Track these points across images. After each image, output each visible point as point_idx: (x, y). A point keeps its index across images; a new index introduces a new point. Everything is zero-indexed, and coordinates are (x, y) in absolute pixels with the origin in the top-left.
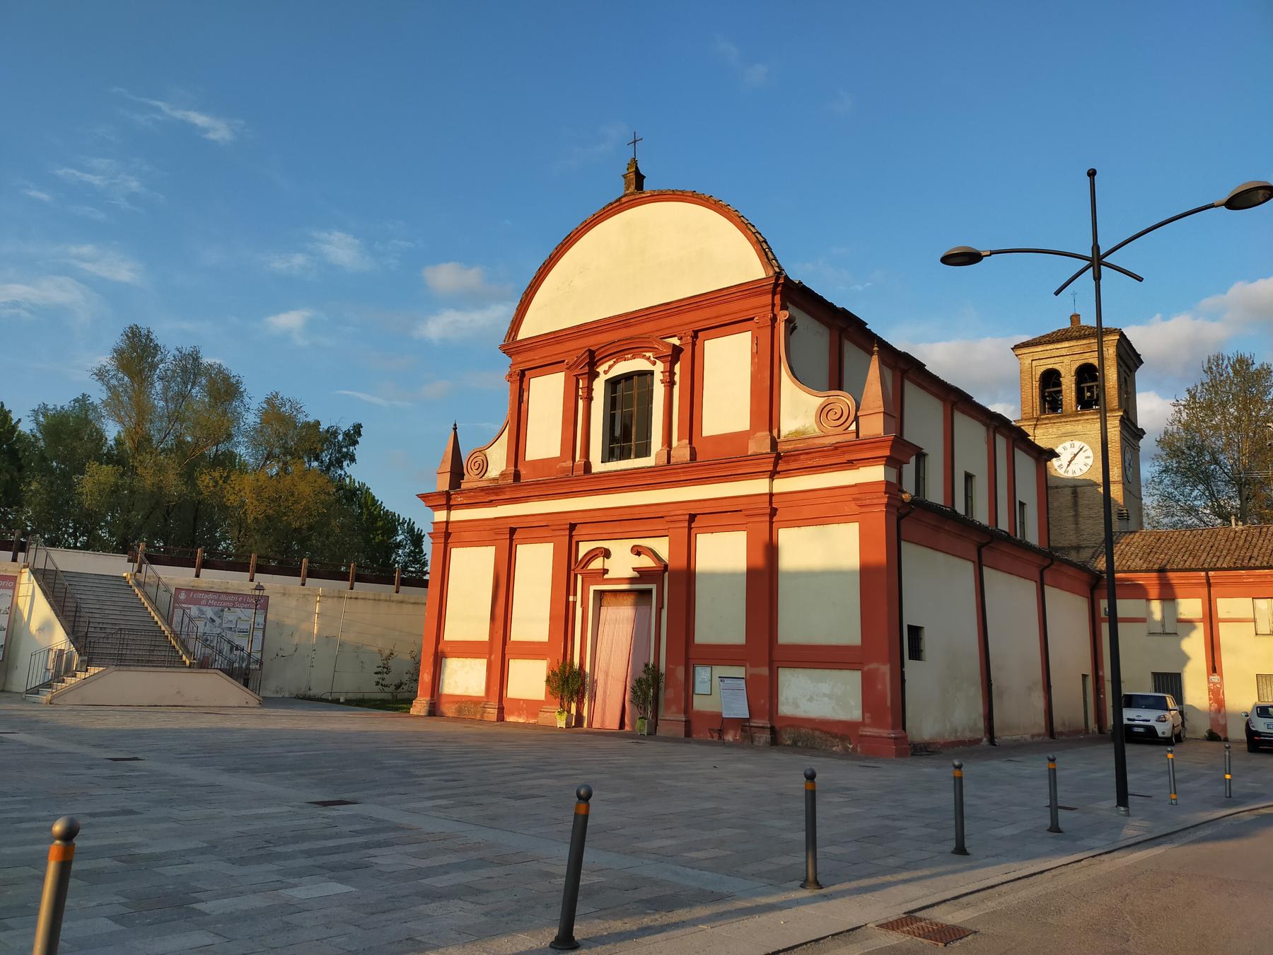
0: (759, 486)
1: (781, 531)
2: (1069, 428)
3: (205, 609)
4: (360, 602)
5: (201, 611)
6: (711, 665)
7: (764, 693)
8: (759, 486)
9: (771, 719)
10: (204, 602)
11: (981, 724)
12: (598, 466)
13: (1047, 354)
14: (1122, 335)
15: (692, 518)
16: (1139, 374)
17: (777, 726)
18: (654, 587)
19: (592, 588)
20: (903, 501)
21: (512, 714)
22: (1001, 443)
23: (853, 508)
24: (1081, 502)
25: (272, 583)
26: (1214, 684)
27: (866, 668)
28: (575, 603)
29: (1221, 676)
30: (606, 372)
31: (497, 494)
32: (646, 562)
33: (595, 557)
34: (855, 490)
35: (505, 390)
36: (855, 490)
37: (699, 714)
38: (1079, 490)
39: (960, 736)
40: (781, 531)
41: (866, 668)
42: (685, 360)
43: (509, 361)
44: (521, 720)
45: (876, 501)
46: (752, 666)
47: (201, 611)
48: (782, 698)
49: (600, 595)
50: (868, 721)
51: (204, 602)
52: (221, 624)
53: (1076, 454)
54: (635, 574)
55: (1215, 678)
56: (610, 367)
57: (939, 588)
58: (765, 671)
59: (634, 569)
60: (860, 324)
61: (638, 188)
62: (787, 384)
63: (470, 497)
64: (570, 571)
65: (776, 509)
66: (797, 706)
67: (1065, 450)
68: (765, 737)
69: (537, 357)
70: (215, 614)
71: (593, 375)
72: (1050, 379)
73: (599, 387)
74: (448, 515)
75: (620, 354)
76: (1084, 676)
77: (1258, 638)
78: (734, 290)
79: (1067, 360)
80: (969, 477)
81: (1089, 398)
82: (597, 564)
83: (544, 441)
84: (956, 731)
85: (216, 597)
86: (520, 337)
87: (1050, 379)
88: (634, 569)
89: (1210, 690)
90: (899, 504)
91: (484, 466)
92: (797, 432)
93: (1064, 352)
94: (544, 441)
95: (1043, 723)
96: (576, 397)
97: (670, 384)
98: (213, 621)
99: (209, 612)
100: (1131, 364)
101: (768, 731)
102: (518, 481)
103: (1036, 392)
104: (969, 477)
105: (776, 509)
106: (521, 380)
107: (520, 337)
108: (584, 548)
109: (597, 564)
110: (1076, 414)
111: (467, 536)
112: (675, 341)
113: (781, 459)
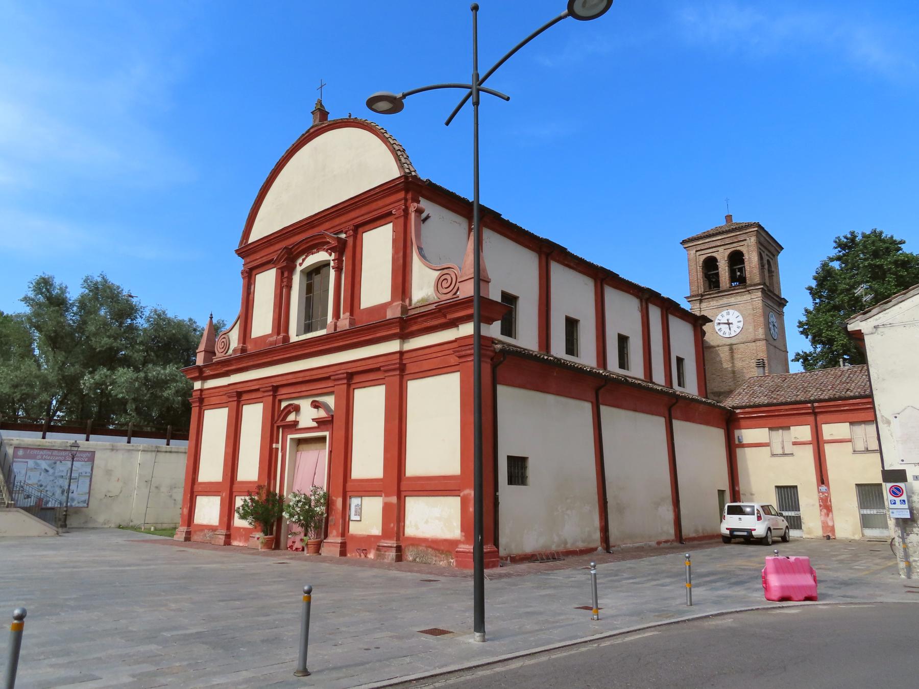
0: (393, 346)
1: (410, 383)
2: (725, 301)
3: (39, 461)
4: (174, 455)
5: (37, 464)
6: (361, 497)
7: (395, 517)
8: (393, 346)
9: (398, 539)
10: (39, 457)
11: (597, 535)
12: (294, 338)
13: (707, 246)
14: (759, 226)
15: (350, 376)
16: (782, 259)
17: (403, 545)
18: (327, 434)
19: (289, 437)
20: (494, 351)
21: (235, 539)
22: (655, 314)
23: (453, 360)
24: (736, 356)
25: (98, 442)
26: (823, 493)
27: (462, 494)
28: (277, 449)
29: (828, 486)
30: (301, 265)
31: (228, 366)
32: (322, 413)
33: (289, 413)
34: (455, 345)
35: (240, 282)
36: (455, 345)
37: (354, 538)
38: (734, 347)
39: (570, 547)
40: (410, 383)
41: (462, 494)
42: (349, 254)
43: (242, 261)
44: (241, 544)
45: (469, 352)
46: (386, 496)
47: (37, 464)
48: (407, 522)
49: (300, 442)
50: (463, 539)
51: (39, 457)
52: (54, 473)
53: (732, 321)
54: (315, 424)
55: (823, 488)
56: (304, 260)
57: (533, 422)
58: (394, 499)
59: (313, 420)
60: (497, 216)
61: (323, 122)
62: (417, 264)
63: (214, 370)
64: (278, 424)
65: (405, 364)
66: (417, 528)
67: (722, 317)
68: (392, 554)
69: (259, 257)
70: (49, 465)
71: (291, 269)
72: (710, 264)
73: (297, 279)
74: (202, 384)
75: (309, 250)
76: (721, 493)
77: (774, 459)
78: (378, 190)
79: (721, 249)
80: (623, 340)
81: (739, 279)
82: (291, 417)
83: (262, 324)
84: (566, 543)
85: (49, 453)
86: (250, 241)
87: (710, 264)
88: (313, 420)
89: (821, 499)
90: (492, 354)
91: (227, 346)
92: (423, 300)
93: (718, 243)
94: (262, 324)
95: (672, 531)
96: (283, 285)
97: (339, 270)
98: (47, 471)
99: (44, 465)
100: (775, 253)
101: (394, 550)
102: (249, 357)
103: (700, 275)
104: (623, 340)
105: (405, 364)
106: (249, 276)
107: (250, 241)
108: (284, 404)
109: (291, 417)
110: (731, 288)
111: (214, 400)
112: (343, 236)
113: (408, 323)
